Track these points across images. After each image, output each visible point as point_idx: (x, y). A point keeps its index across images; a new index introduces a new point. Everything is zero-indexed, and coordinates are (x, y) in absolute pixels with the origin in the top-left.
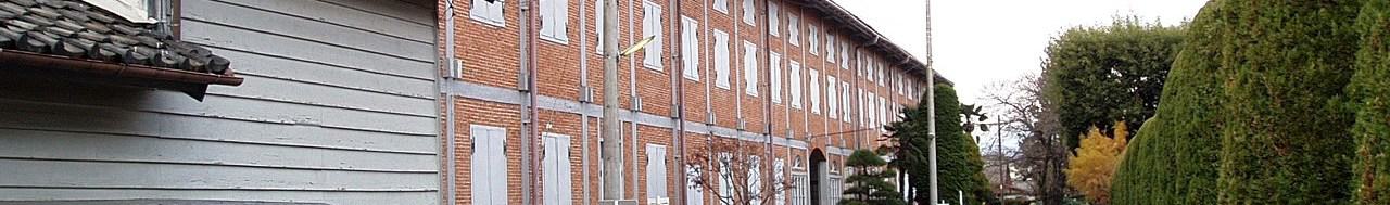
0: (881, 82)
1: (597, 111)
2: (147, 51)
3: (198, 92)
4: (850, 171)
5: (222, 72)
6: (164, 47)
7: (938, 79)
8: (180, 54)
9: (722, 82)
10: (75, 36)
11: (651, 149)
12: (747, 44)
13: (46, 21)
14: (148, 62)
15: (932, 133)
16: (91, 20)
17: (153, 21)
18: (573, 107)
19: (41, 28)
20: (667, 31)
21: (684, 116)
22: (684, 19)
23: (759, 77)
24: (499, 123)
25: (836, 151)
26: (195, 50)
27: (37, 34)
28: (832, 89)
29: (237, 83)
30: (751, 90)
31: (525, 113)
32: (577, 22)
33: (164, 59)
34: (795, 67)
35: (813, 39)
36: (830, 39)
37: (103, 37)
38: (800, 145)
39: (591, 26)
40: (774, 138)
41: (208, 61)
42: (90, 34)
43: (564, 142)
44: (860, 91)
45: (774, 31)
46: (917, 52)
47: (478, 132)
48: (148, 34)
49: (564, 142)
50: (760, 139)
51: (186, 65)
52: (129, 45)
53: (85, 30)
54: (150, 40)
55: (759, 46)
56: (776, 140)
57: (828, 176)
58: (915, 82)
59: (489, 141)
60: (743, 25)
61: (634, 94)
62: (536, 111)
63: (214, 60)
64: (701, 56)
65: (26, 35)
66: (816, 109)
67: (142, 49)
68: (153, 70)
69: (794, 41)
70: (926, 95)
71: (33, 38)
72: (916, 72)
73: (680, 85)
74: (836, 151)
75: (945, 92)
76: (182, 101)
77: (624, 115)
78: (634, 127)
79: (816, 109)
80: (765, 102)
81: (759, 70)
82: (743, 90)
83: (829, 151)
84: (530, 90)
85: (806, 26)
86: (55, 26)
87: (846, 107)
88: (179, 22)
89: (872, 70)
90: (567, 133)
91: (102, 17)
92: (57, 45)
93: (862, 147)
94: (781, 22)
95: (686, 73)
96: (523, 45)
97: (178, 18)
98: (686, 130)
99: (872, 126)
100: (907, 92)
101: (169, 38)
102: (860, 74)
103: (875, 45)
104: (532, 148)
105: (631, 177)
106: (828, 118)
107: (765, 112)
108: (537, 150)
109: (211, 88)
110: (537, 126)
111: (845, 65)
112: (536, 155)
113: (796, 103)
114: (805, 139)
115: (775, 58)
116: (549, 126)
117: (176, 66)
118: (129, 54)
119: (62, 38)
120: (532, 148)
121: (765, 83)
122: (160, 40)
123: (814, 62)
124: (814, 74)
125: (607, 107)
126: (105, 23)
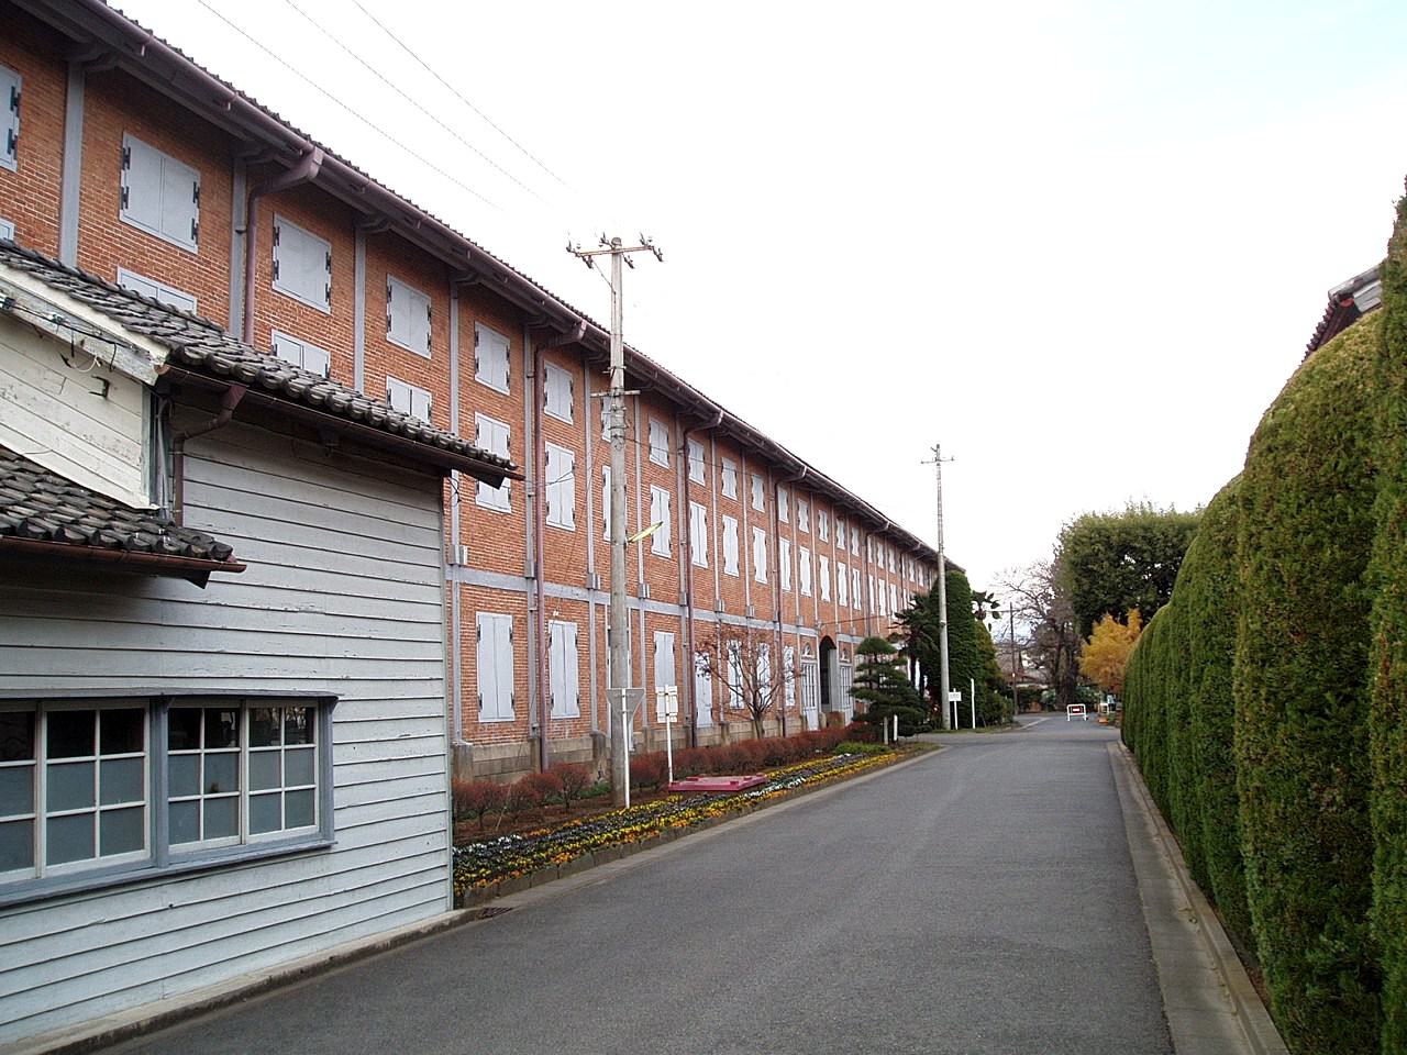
2: (148, 537)
3: (201, 579)
4: (860, 659)
5: (225, 559)
6: (166, 534)
7: (949, 566)
8: (182, 540)
11: (659, 636)
13: (46, 507)
14: (150, 549)
15: (944, 620)
16: (93, 506)
17: (155, 507)
18: (580, 593)
19: (42, 514)
20: (675, 518)
22: (692, 505)
23: (769, 564)
24: (505, 610)
25: (846, 638)
26: (198, 536)
27: (38, 520)
29: (240, 569)
30: (761, 577)
31: (531, 600)
32: (584, 508)
33: (166, 546)
34: (805, 553)
35: (823, 526)
36: (841, 525)
37: (104, 523)
38: (810, 633)
40: (784, 626)
41: (210, 548)
42: (91, 520)
43: (571, 629)
44: (871, 578)
45: (783, 517)
46: (928, 539)
47: (484, 619)
48: (149, 520)
49: (571, 629)
50: (769, 626)
52: (131, 532)
53: (86, 516)
54: (151, 527)
55: (768, 532)
56: (786, 628)
59: (495, 629)
60: (752, 512)
61: (641, 581)
63: (216, 547)
64: (710, 543)
65: (26, 521)
66: (826, 596)
67: (143, 535)
69: (803, 527)
70: (937, 582)
71: (34, 524)
72: (927, 559)
73: (688, 572)
74: (846, 638)
79: (826, 596)
80: (774, 590)
81: (768, 557)
83: (840, 639)
84: (536, 577)
86: (55, 512)
87: (857, 595)
89: (882, 556)
90: (574, 620)
91: (103, 503)
92: (57, 532)
93: (872, 635)
94: (790, 508)
95: (695, 560)
96: (530, 531)
97: (180, 504)
98: (694, 617)
99: (883, 613)
100: (918, 579)
101: (171, 524)
102: (870, 560)
104: (538, 636)
105: (639, 665)
109: (213, 575)
110: (543, 614)
111: (855, 552)
112: (543, 642)
113: (806, 590)
114: (815, 627)
115: (784, 545)
116: (556, 613)
117: (178, 553)
118: (130, 540)
119: (63, 524)
120: (538, 636)
121: (774, 570)
123: (824, 549)
124: (824, 561)
125: (614, 595)
126: (106, 509)
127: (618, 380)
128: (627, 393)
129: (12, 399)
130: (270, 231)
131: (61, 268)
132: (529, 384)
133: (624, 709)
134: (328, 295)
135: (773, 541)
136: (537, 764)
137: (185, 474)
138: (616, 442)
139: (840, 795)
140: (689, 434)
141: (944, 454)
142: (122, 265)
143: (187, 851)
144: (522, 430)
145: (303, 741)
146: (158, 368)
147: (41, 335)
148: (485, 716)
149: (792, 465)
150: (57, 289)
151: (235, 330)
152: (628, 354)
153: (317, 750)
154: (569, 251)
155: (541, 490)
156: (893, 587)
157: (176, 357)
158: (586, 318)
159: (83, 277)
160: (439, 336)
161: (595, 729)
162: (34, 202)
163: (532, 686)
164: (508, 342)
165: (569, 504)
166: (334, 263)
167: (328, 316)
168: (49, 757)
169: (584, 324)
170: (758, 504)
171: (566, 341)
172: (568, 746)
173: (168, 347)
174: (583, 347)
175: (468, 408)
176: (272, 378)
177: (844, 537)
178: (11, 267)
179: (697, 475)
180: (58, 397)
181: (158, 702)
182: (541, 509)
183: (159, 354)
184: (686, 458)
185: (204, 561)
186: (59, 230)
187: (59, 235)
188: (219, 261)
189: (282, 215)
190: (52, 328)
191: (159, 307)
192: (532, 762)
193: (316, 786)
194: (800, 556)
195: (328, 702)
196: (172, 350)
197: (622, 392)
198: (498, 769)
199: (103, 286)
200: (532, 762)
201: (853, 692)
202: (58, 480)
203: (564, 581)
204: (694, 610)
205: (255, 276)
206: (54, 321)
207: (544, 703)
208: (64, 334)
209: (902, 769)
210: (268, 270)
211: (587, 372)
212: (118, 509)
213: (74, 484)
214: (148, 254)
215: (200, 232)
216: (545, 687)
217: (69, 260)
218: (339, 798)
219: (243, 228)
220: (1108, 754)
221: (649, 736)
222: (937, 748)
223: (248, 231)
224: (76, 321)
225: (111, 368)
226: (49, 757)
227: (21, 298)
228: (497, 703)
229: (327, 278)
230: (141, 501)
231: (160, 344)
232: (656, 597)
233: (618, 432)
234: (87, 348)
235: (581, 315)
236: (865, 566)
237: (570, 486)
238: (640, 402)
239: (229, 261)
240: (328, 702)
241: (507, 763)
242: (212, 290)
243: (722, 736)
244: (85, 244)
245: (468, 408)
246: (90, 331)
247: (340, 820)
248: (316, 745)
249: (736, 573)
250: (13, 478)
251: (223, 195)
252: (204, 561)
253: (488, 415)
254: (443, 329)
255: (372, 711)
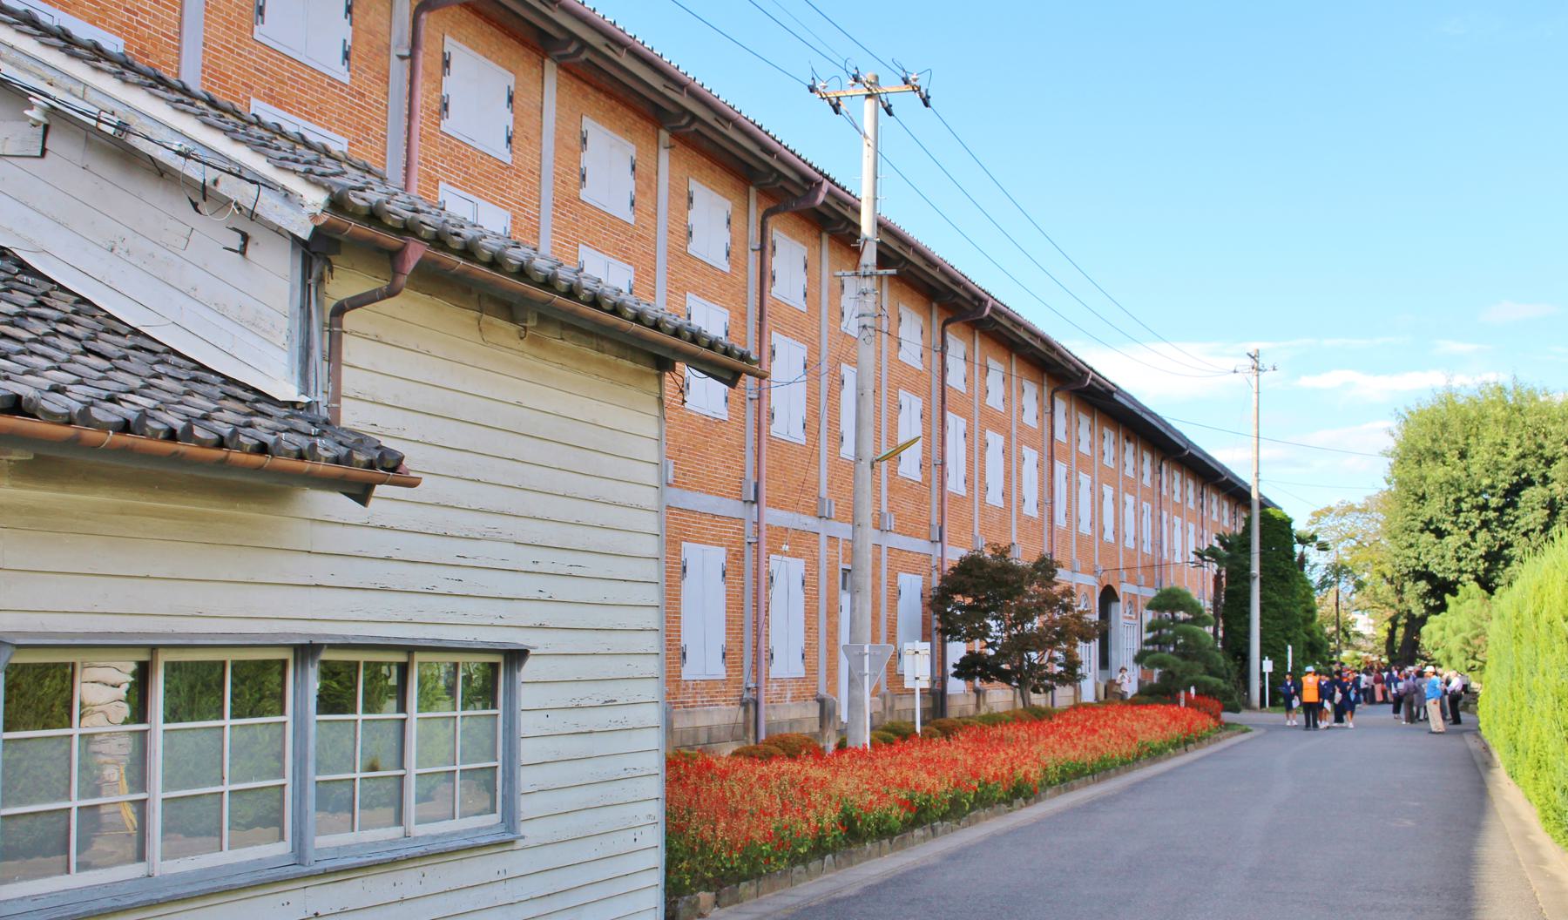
0: (1191, 505)
1: (843, 531)
2: (297, 439)
3: (362, 494)
4: (1149, 616)
5: (394, 470)
6: (319, 435)
7: (1265, 503)
8: (340, 443)
9: (995, 498)
10: (206, 418)
12: (904, 397)
13: (168, 397)
14: (301, 456)
15: (1256, 570)
16: (228, 396)
17: (305, 399)
18: (810, 523)
19: (164, 406)
20: (456, 243)
21: (763, 500)
22: (949, 416)
23: (1041, 493)
24: (717, 541)
25: (1132, 589)
26: (361, 440)
27: (158, 413)
28: (1129, 513)
29: (412, 483)
30: (1030, 509)
31: (749, 529)
32: (817, 416)
33: (320, 451)
34: (1085, 479)
35: (1108, 446)
36: (1130, 447)
37: (243, 420)
39: (834, 422)
41: (377, 455)
42: (227, 415)
43: (797, 567)
44: (1165, 514)
45: (1060, 435)
46: (1244, 474)
48: (298, 417)
49: (797, 567)
51: (347, 460)
52: (275, 432)
53: (220, 410)
54: (302, 425)
55: (1041, 453)
57: (1122, 621)
58: (1047, 392)
59: (706, 561)
60: (1022, 427)
61: (884, 509)
62: (763, 528)
63: (385, 452)
64: (970, 464)
65: (144, 414)
66: (1109, 536)
67: (292, 436)
68: (307, 466)
69: (1084, 448)
70: (1248, 521)
71: (153, 418)
72: (1236, 494)
74: (1132, 589)
75: (1277, 530)
76: (337, 504)
77: (870, 536)
78: (823, 541)
79: (1109, 536)
80: (1047, 525)
81: (1041, 484)
82: (1019, 508)
83: (1124, 589)
84: (756, 501)
85: (1101, 430)
86: (180, 403)
87: (1147, 535)
88: (338, 401)
89: (1179, 487)
90: (799, 556)
91: (239, 392)
92: (184, 429)
93: (1166, 586)
94: (1069, 423)
96: (750, 443)
97: (337, 396)
98: (766, 520)
99: (1178, 559)
100: (1222, 518)
101: (327, 422)
102: (1164, 492)
103: (815, 211)
104: (757, 576)
106: (982, 510)
107: (1046, 537)
108: (764, 578)
109: (379, 490)
110: (764, 547)
111: (1147, 481)
112: (762, 583)
113: (1085, 528)
115: (1061, 469)
116: (786, 548)
117: (337, 460)
118: (277, 443)
119: (190, 420)
120: (757, 576)
122: (313, 424)
123: (1111, 477)
124: (1108, 491)
125: (856, 525)
126: (243, 401)
127: (869, 256)
128: (881, 272)
129: (123, 254)
130: (440, 58)
131: (185, 91)
132: (753, 259)
133: (867, 670)
134: (509, 140)
135: (1047, 463)
136: (751, 735)
137: (345, 357)
138: (865, 333)
139: (1134, 788)
140: (949, 327)
141: (1264, 361)
142: (258, 97)
143: (330, 841)
144: (744, 316)
145: (478, 705)
146: (314, 217)
147: (161, 172)
148: (689, 672)
149: (968, 297)
150: (184, 111)
151: (394, 172)
152: (882, 227)
153: (500, 719)
154: (812, 89)
155: (765, 393)
156: (1192, 527)
157: (337, 204)
158: (827, 177)
159: (212, 103)
160: (644, 194)
161: (823, 692)
162: (149, 13)
163: (748, 637)
164: (728, 205)
165: (800, 412)
166: (517, 100)
167: (508, 167)
168: (166, 721)
169: (826, 185)
170: (1030, 417)
171: (803, 205)
172: (789, 714)
173: (328, 189)
174: (821, 214)
175: (678, 288)
176: (458, 235)
177: (1134, 463)
178: (125, 82)
179: (956, 378)
180: (183, 254)
181: (306, 651)
182: (763, 416)
183: (316, 199)
184: (943, 357)
185: (368, 471)
186: (179, 49)
187: (179, 55)
188: (376, 93)
189: (454, 37)
190: (177, 163)
191: (308, 145)
192: (746, 730)
193: (499, 764)
194: (1078, 484)
195: (516, 656)
196: (332, 193)
197: (874, 270)
198: (703, 738)
199: (237, 114)
200: (746, 730)
201: (1139, 659)
202: (182, 362)
203: (795, 507)
204: (946, 546)
205: (419, 113)
206: (179, 153)
207: (761, 656)
208: (193, 171)
209: (1208, 757)
210: (436, 106)
211: (752, 190)
212: (257, 401)
213: (203, 367)
214: (290, 80)
215: (353, 56)
216: (763, 639)
217: (192, 77)
218: (526, 778)
219: (406, 52)
220: (1469, 751)
221: (889, 704)
222: (1246, 731)
223: (412, 56)
224: (209, 154)
225: (253, 216)
226: (166, 721)
227: (136, 124)
228: (705, 661)
229: (507, 118)
230: (287, 390)
231: (317, 184)
232: (901, 530)
233: (868, 321)
234: (222, 189)
235: (821, 173)
236: (1159, 502)
237: (800, 390)
238: (890, 284)
239: (387, 94)
240: (516, 656)
241: (715, 732)
242: (367, 129)
243: (978, 706)
244: (211, 71)
245: (678, 288)
246: (227, 166)
247: (526, 806)
248: (500, 711)
249: (1000, 503)
250: (126, 358)
251: (382, 9)
252: (368, 471)
253: (703, 295)
254: (649, 186)
255: (569, 668)
